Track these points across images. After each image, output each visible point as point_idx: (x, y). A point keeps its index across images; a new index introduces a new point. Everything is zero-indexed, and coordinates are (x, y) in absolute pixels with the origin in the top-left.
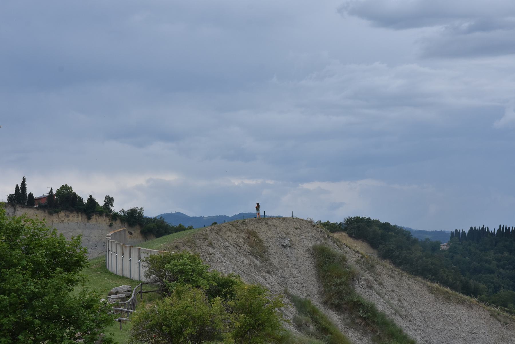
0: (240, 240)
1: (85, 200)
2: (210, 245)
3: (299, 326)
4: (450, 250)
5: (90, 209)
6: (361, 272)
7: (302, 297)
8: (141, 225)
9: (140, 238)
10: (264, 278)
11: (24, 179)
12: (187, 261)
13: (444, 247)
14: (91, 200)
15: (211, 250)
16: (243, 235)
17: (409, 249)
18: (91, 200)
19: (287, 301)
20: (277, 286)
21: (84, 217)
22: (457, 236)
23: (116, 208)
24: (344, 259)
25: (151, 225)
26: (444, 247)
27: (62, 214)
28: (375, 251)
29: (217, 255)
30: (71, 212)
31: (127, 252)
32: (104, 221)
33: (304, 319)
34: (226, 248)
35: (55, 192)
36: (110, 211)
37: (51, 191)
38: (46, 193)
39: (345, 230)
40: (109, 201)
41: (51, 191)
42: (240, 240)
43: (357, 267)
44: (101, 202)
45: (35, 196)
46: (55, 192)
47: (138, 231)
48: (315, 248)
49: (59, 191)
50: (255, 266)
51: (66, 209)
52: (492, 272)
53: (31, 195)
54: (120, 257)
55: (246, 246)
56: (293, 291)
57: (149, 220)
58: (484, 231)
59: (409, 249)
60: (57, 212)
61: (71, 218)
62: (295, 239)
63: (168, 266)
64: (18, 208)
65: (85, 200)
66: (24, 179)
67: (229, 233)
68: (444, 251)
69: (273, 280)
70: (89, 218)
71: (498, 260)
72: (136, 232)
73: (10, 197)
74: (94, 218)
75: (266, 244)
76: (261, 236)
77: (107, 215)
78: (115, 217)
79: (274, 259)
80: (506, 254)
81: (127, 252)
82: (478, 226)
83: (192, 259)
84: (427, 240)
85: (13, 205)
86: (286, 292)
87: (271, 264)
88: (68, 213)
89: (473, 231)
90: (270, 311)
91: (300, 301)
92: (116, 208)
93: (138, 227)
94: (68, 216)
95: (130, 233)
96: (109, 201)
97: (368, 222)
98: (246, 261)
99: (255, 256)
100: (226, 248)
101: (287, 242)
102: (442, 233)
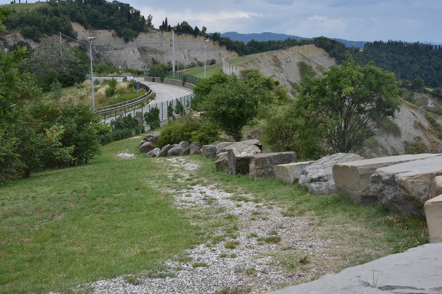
0: (270, 60)
1: (194, 28)
2: (259, 62)
3: (293, 93)
4: (364, 52)
5: (196, 33)
6: (318, 72)
7: (294, 82)
8: (219, 40)
9: (219, 46)
10: (280, 74)
11: (166, 18)
12: (254, 73)
13: (361, 50)
14: (196, 28)
15: (260, 64)
16: (271, 57)
17: (344, 52)
18: (196, 28)
19: (288, 83)
20: (284, 78)
21: (193, 36)
22: (368, 45)
23: (208, 32)
24: (311, 67)
25: (224, 41)
26: (361, 50)
27: (183, 35)
28: (328, 53)
29: (262, 66)
30: (188, 34)
31: (231, 67)
32: (202, 38)
33: (294, 90)
34: (265, 63)
35: (180, 25)
36: (205, 34)
37: (178, 24)
38: (176, 25)
39: (314, 43)
40: (205, 29)
41: (178, 24)
42: (270, 60)
43: (316, 70)
44: (201, 29)
45: (171, 26)
46: (180, 25)
47: (218, 43)
48: (299, 63)
49: (182, 24)
50: (276, 70)
51: (185, 33)
52: (383, 62)
53: (169, 26)
54: (229, 69)
55: (272, 62)
56: (290, 80)
57: (222, 38)
58: (381, 43)
59: (344, 52)
60: (181, 34)
61: (187, 37)
62: (292, 59)
63: (248, 74)
64: (164, 32)
65: (194, 28)
66: (166, 18)
67: (266, 57)
68: (361, 52)
69: (283, 75)
70: (196, 37)
71: (387, 57)
72: (217, 43)
73: (160, 27)
74: (198, 37)
75: (280, 61)
76: (279, 58)
77: (204, 36)
78: (207, 36)
79: (283, 67)
80: (391, 54)
81: (231, 67)
82: (378, 40)
83: (256, 71)
84: (353, 47)
85: (162, 31)
86: (288, 80)
87: (282, 69)
88: (186, 34)
89: (375, 42)
90: (285, 93)
91: (293, 84)
92: (208, 32)
93: (218, 41)
94: (186, 36)
95: (214, 44)
96: (205, 29)
97: (325, 39)
98: (273, 68)
99: (276, 66)
100: (265, 63)
101: (289, 60)
102: (362, 42)
